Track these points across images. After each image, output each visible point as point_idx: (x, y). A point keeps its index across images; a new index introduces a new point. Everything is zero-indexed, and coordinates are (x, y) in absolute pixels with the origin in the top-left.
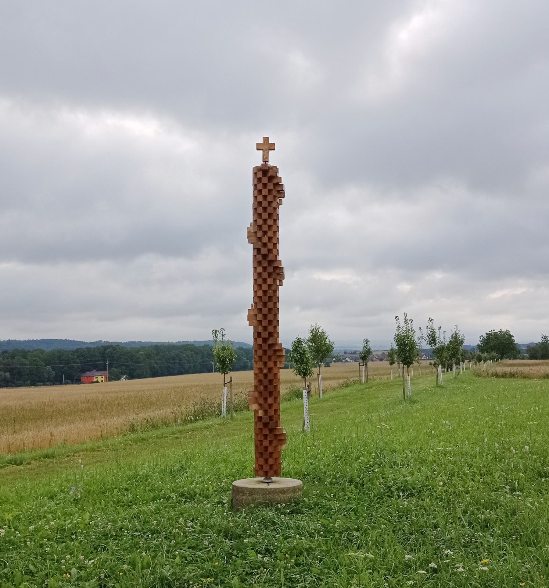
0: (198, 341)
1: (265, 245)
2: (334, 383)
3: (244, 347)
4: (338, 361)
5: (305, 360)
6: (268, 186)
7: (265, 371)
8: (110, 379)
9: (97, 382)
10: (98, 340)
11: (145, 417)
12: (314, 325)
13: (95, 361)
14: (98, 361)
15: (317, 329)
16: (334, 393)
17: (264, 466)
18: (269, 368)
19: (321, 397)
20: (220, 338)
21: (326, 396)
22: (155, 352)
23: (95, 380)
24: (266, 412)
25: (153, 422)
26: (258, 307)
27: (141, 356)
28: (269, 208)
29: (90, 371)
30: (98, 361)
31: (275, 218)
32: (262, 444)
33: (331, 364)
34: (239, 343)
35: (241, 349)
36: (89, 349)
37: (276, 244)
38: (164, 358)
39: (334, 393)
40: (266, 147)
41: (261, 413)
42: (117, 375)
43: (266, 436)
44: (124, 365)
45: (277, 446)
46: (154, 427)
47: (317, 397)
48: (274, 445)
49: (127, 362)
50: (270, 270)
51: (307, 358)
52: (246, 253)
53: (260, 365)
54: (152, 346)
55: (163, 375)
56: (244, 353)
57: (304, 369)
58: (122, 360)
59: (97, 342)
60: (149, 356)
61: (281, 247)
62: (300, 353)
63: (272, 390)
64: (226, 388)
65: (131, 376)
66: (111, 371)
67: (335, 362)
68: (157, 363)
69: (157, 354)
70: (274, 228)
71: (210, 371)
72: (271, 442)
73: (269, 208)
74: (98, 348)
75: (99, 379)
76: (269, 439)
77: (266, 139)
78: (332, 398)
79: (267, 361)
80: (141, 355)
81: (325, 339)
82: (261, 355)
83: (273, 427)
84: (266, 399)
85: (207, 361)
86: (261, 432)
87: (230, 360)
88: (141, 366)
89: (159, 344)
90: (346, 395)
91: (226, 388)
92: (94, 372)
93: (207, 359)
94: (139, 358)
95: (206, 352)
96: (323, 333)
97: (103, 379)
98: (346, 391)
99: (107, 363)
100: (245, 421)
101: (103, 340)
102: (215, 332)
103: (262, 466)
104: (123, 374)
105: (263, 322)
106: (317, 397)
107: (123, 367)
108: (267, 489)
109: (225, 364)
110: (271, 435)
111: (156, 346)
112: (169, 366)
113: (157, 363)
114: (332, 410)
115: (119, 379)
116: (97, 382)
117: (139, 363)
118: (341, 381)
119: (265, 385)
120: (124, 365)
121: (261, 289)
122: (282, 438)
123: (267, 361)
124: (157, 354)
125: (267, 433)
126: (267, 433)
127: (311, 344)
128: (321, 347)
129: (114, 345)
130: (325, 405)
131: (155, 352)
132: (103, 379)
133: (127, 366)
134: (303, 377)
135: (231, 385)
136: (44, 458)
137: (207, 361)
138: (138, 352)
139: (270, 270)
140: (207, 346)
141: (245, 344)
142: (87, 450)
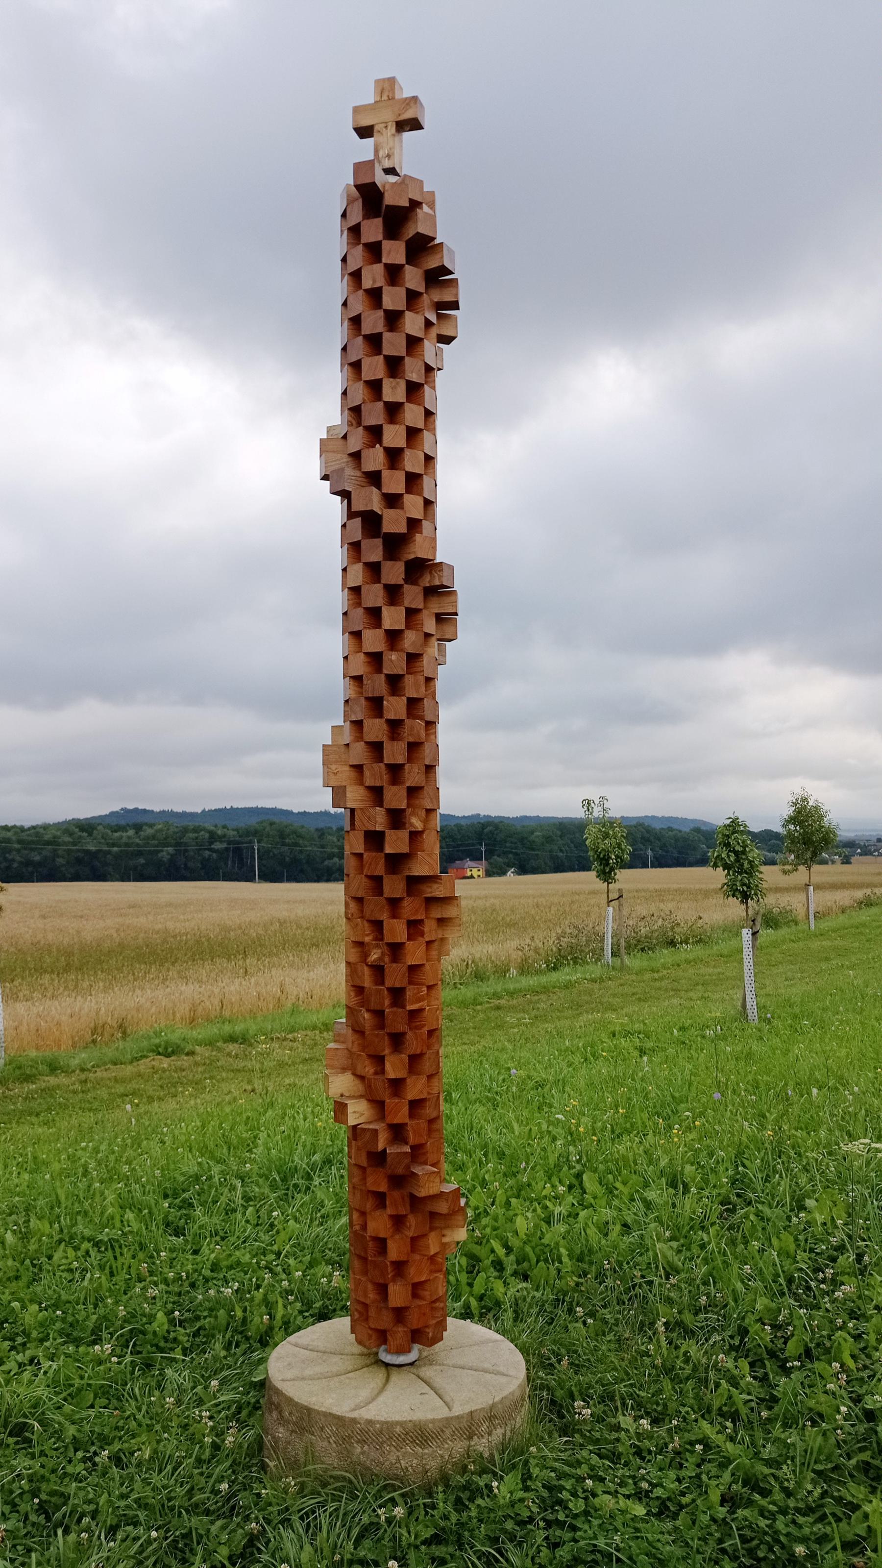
0: (627, 817)
2: (844, 897)
3: (703, 828)
4: (866, 854)
5: (746, 865)
8: (489, 874)
9: (472, 877)
10: (474, 813)
11: (465, 958)
12: (798, 791)
13: (468, 845)
14: (473, 845)
15: (805, 800)
16: (842, 919)
19: (813, 927)
20: (597, 812)
21: (824, 925)
22: (559, 833)
23: (469, 874)
25: (477, 966)
27: (537, 840)
29: (461, 859)
30: (473, 845)
33: (853, 859)
34: (693, 821)
35: (697, 830)
36: (459, 827)
38: (572, 842)
39: (842, 919)
41: (358, 1112)
42: (501, 868)
43: (380, 1199)
44: (511, 852)
45: (424, 1236)
46: (479, 976)
47: (806, 927)
48: (411, 1234)
49: (516, 848)
51: (750, 862)
54: (554, 824)
55: (572, 869)
56: (702, 838)
57: (743, 884)
58: (508, 845)
59: (472, 816)
60: (548, 839)
62: (736, 853)
64: (611, 909)
65: (523, 870)
66: (492, 861)
67: (861, 855)
68: (561, 851)
69: (561, 837)
71: (645, 866)
74: (473, 825)
75: (475, 872)
76: (390, 1211)
78: (834, 931)
80: (538, 836)
81: (821, 818)
85: (641, 850)
87: (617, 857)
88: (537, 855)
89: (565, 821)
90: (864, 925)
91: (611, 909)
92: (469, 863)
93: (641, 846)
94: (534, 841)
95: (639, 835)
96: (817, 808)
97: (480, 873)
98: (864, 916)
99: (483, 850)
100: (647, 976)
101: (482, 814)
102: (588, 804)
104: (509, 866)
106: (806, 927)
107: (510, 856)
108: (354, 1421)
109: (608, 864)
111: (560, 824)
112: (580, 856)
113: (561, 851)
114: (827, 959)
115: (503, 873)
116: (472, 877)
117: (533, 849)
118: (859, 894)
120: (511, 852)
124: (561, 837)
127: (792, 827)
128: (812, 833)
129: (496, 821)
130: (815, 944)
131: (559, 833)
132: (480, 873)
133: (516, 854)
134: (742, 902)
135: (620, 905)
136: (226, 1041)
137: (641, 850)
138: (532, 832)
140: (642, 825)
141: (704, 823)
142: (314, 1028)
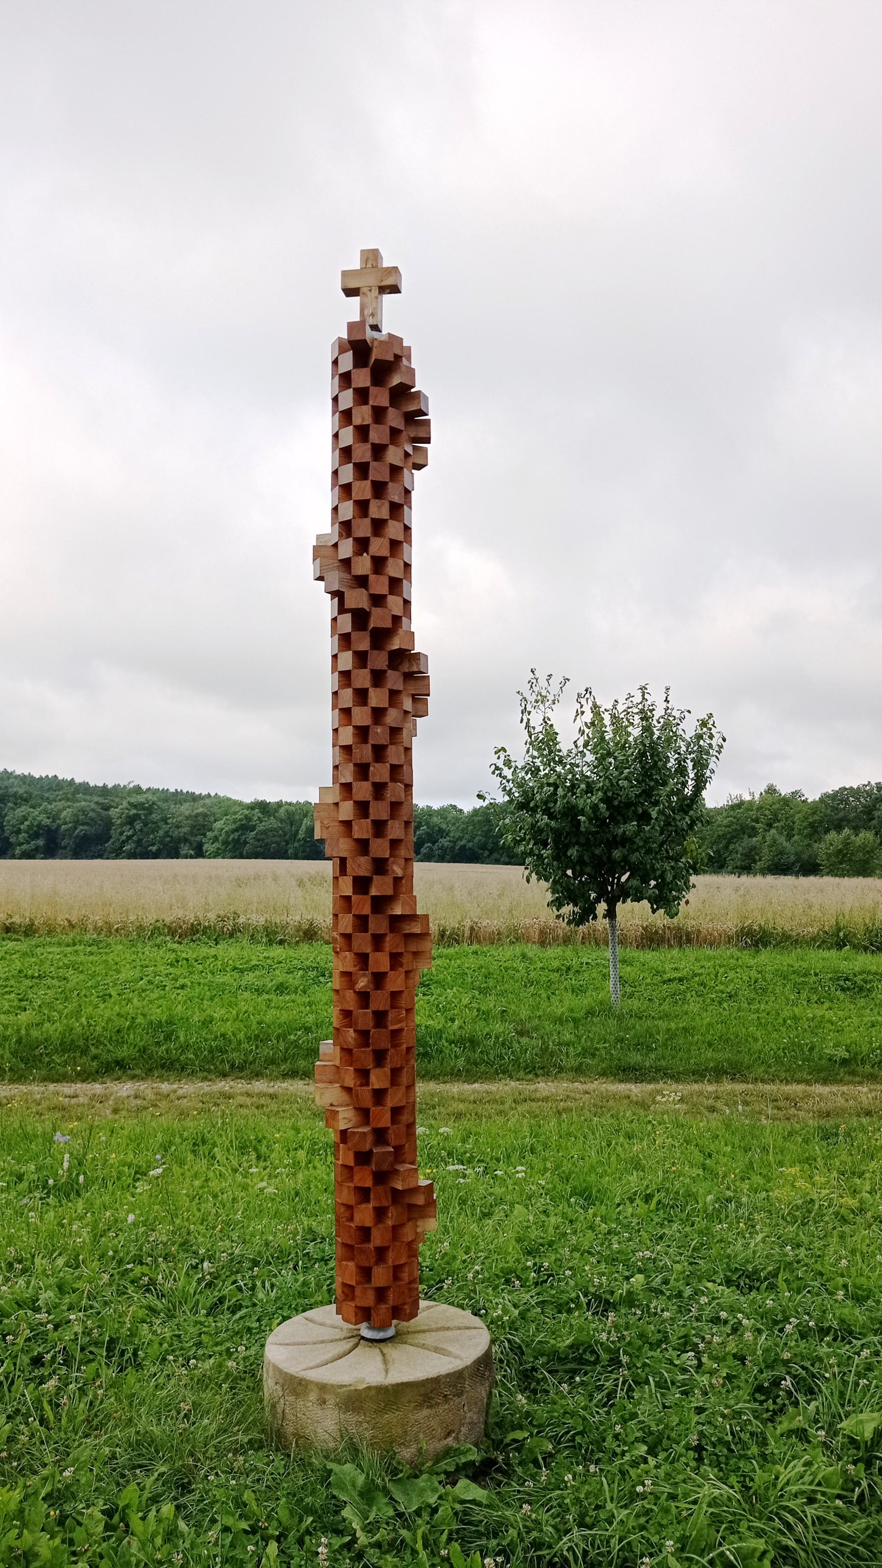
1: (362, 582)
6: (380, 407)
7: (362, 983)
17: (358, 1292)
18: (374, 974)
24: (364, 1114)
26: (343, 781)
28: (391, 523)
31: (396, 499)
32: (351, 1219)
37: (399, 581)
40: (371, 281)
50: (379, 660)
52: (312, 614)
53: (348, 962)
61: (419, 589)
63: (385, 1044)
70: (393, 530)
72: (380, 1213)
73: (391, 523)
77: (371, 257)
79: (368, 950)
82: (349, 930)
83: (385, 1167)
84: (363, 1074)
86: (351, 1178)
103: (348, 899)
105: (355, 827)
110: (380, 1188)
119: (360, 1027)
121: (351, 798)
122: (420, 1200)
123: (368, 950)
125: (368, 1183)
126: (368, 1183)
139: (379, 660)
